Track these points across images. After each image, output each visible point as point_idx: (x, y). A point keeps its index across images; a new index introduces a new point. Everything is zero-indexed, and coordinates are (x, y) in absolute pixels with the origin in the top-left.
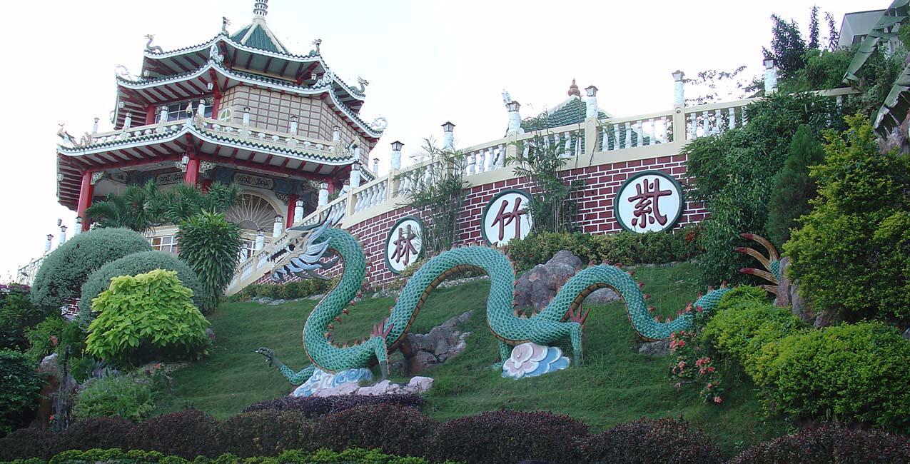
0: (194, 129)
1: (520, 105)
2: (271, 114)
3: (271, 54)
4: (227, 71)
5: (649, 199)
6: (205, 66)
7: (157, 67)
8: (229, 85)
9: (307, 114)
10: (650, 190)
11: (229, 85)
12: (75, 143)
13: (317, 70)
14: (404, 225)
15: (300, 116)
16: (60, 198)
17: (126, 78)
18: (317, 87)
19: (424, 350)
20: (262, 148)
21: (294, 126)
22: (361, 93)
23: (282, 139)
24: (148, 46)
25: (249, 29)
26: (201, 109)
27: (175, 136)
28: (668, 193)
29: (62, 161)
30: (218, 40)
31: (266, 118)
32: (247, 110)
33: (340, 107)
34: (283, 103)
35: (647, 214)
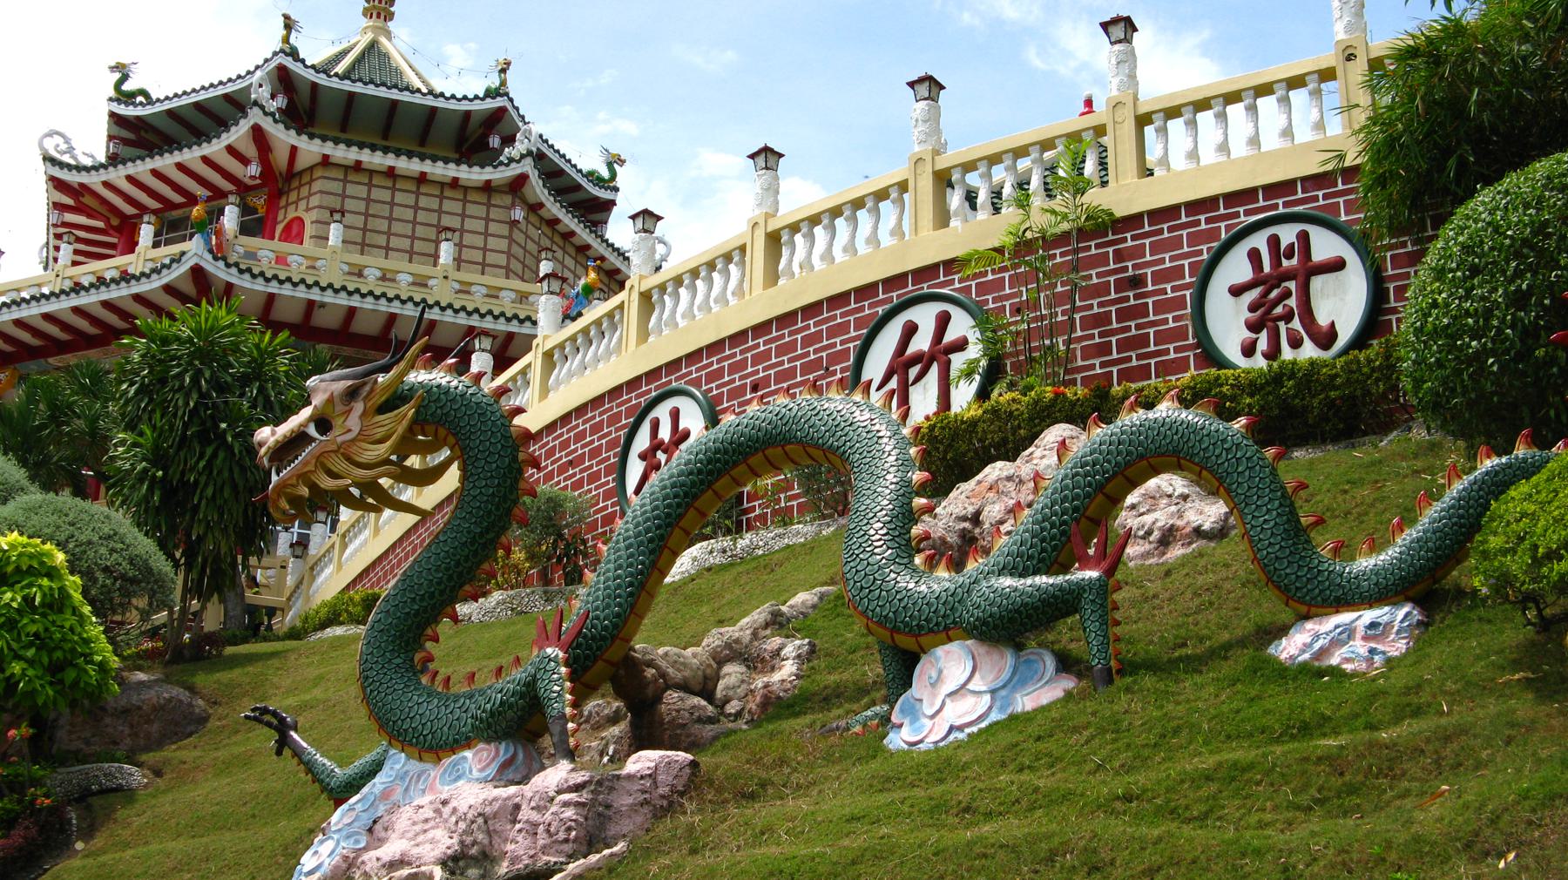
0: (209, 257)
2: (398, 227)
3: (394, 95)
4: (293, 132)
5: (1287, 284)
6: (242, 122)
7: (138, 132)
9: (479, 225)
10: (1285, 263)
11: (302, 162)
13: (503, 127)
14: (662, 412)
17: (66, 159)
18: (501, 163)
20: (370, 299)
21: (446, 251)
22: (609, 184)
23: (421, 282)
26: (230, 218)
27: (167, 277)
28: (1338, 265)
30: (273, 64)
32: (337, 216)
34: (423, 201)
35: (1282, 326)
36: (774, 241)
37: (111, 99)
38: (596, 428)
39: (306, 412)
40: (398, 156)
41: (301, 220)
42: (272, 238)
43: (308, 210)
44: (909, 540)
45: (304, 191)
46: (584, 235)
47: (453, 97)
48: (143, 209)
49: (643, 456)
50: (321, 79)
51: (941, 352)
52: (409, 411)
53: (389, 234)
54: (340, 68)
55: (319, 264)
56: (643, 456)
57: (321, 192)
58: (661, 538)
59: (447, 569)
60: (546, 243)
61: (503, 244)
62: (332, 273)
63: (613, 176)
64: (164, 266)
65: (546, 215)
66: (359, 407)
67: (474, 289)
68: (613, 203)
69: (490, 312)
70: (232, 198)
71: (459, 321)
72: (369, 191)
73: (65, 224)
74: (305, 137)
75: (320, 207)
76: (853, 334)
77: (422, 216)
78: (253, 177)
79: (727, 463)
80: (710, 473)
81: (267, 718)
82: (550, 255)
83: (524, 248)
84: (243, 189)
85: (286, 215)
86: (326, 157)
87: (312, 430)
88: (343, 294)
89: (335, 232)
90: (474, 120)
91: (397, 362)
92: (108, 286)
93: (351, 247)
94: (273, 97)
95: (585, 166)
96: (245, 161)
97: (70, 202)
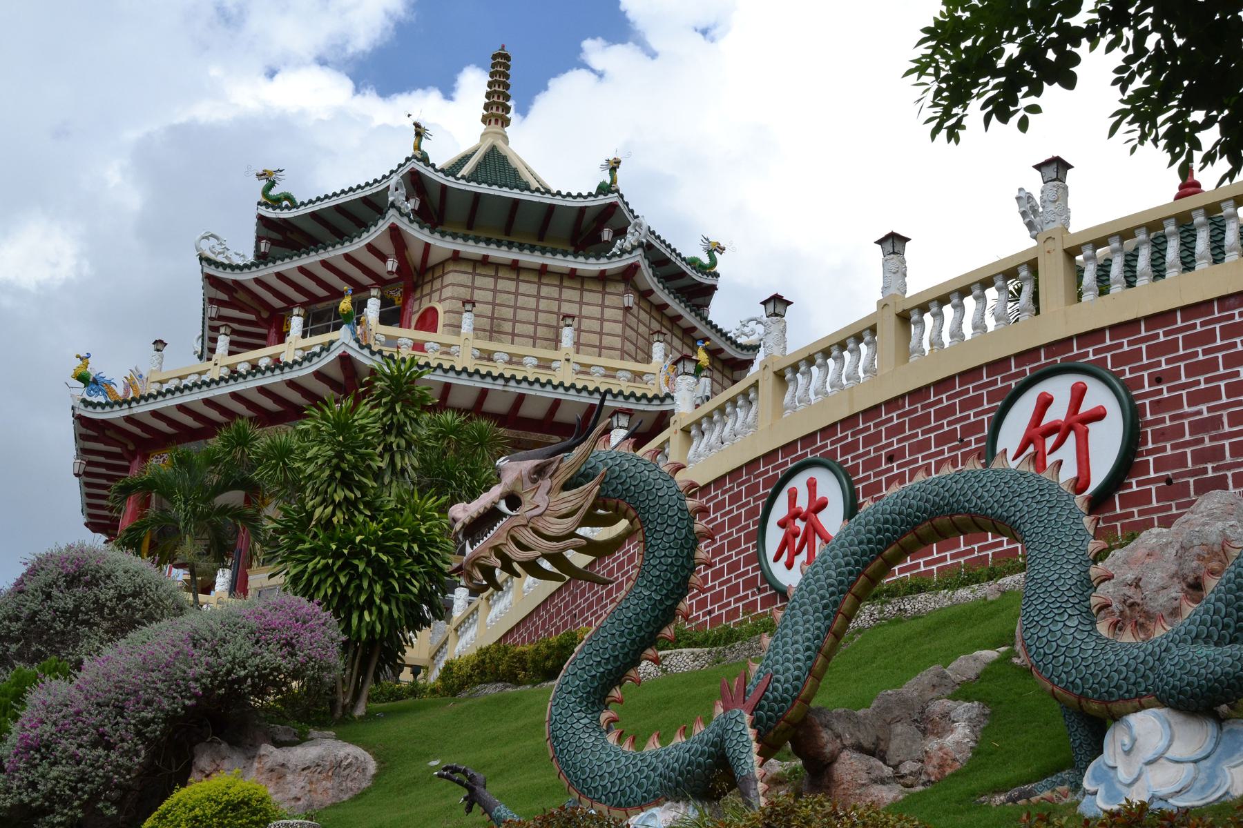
0: (356, 346)
1: (1068, 166)
3: (516, 194)
4: (426, 231)
6: (381, 222)
7: (282, 233)
8: (434, 259)
11: (434, 259)
12: (114, 393)
13: (614, 220)
14: (799, 483)
15: (581, 317)
16: (90, 515)
17: (220, 259)
18: (614, 255)
19: (859, 748)
22: (709, 269)
24: (265, 192)
25: (471, 156)
26: (373, 308)
27: (317, 364)
29: (83, 431)
30: (406, 170)
31: (476, 285)
32: (468, 307)
33: (662, 295)
36: (904, 318)
37: (259, 204)
38: (735, 498)
39: (496, 491)
40: (521, 250)
41: (434, 311)
42: (409, 327)
43: (440, 301)
44: (1089, 608)
45: (437, 284)
46: (690, 319)
47: (559, 193)
48: (291, 304)
49: (782, 524)
50: (450, 182)
51: (1079, 422)
52: (592, 487)
53: (514, 321)
54: (465, 171)
55: (453, 349)
56: (782, 524)
57: (454, 285)
58: (835, 603)
59: (630, 634)
60: (656, 326)
61: (618, 328)
62: (465, 359)
63: (714, 263)
64: (314, 354)
65: (656, 302)
66: (546, 483)
67: (593, 370)
68: (713, 288)
69: (585, 388)
70: (374, 292)
71: (583, 400)
72: (473, 280)
73: (221, 318)
74: (437, 235)
75: (452, 298)
76: (986, 406)
77: (543, 304)
78: (390, 273)
79: (895, 532)
80: (880, 542)
81: (457, 776)
82: (661, 338)
83: (636, 332)
84: (380, 282)
85: (417, 308)
86: (456, 252)
87: (503, 506)
88: (477, 378)
89: (467, 321)
90: (588, 216)
91: (578, 444)
92: (263, 373)
93: (481, 334)
94: (407, 199)
95: (687, 254)
96: (384, 258)
97: (225, 297)
